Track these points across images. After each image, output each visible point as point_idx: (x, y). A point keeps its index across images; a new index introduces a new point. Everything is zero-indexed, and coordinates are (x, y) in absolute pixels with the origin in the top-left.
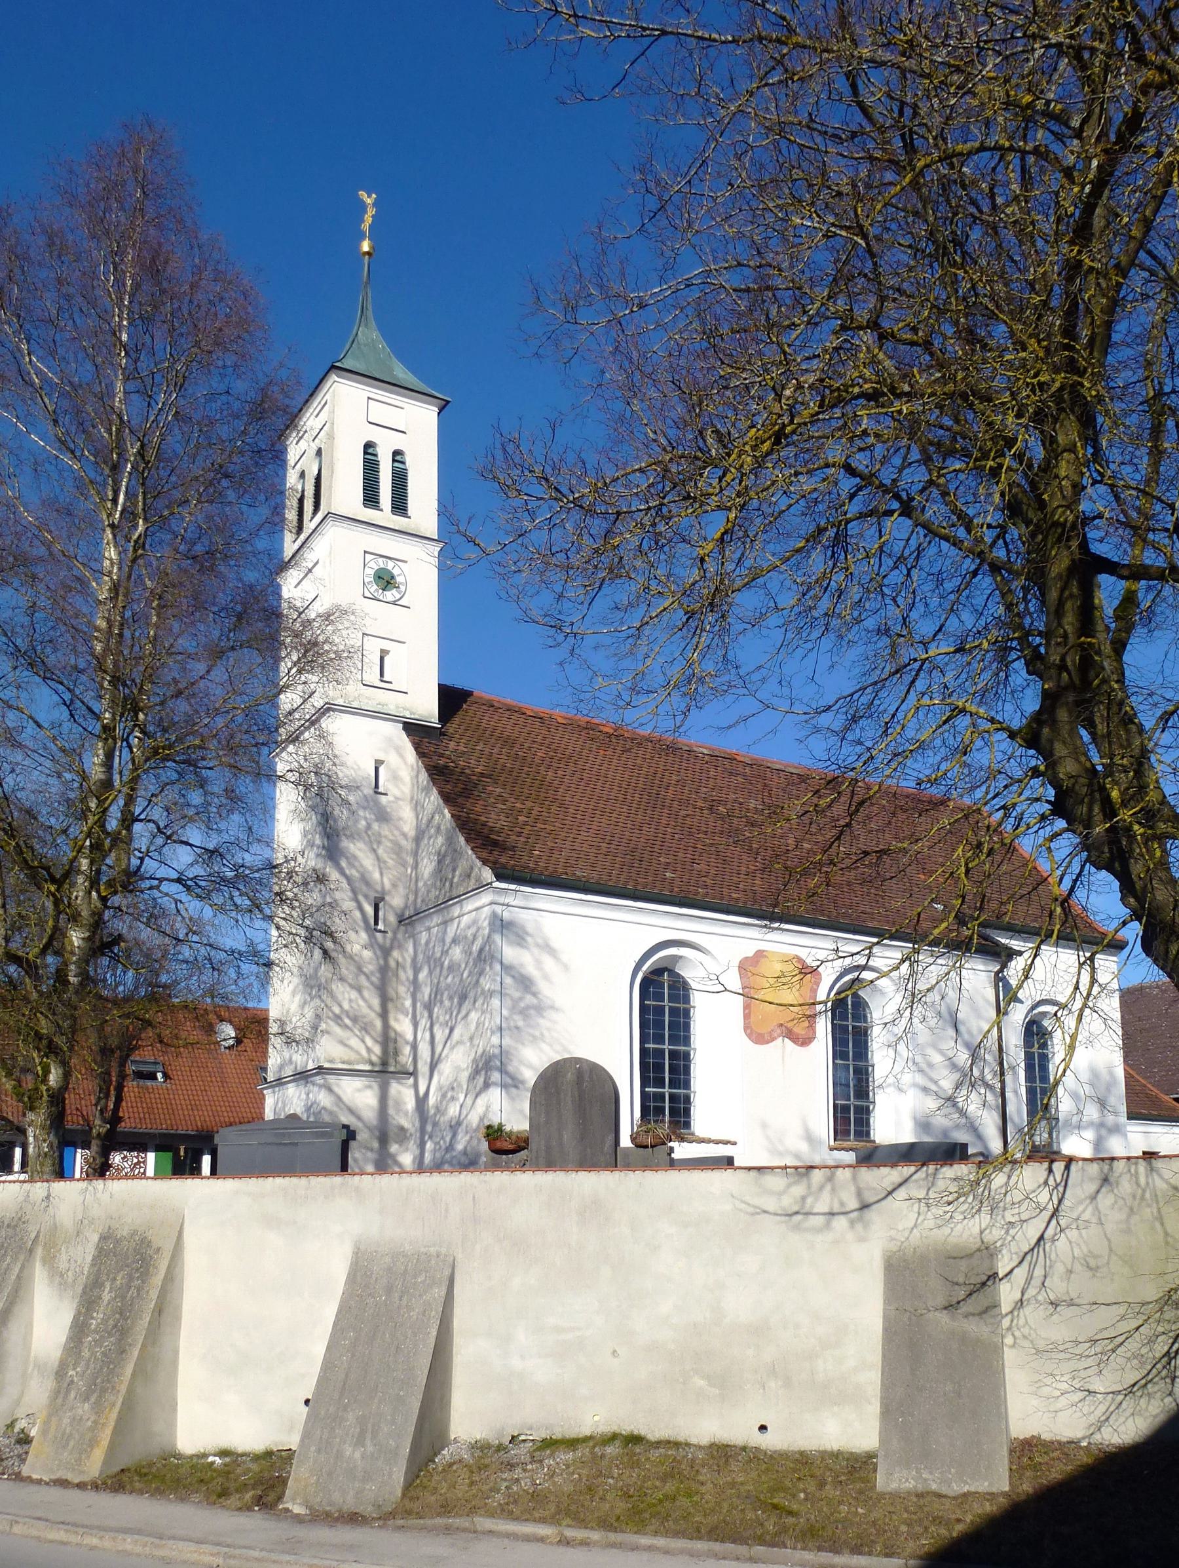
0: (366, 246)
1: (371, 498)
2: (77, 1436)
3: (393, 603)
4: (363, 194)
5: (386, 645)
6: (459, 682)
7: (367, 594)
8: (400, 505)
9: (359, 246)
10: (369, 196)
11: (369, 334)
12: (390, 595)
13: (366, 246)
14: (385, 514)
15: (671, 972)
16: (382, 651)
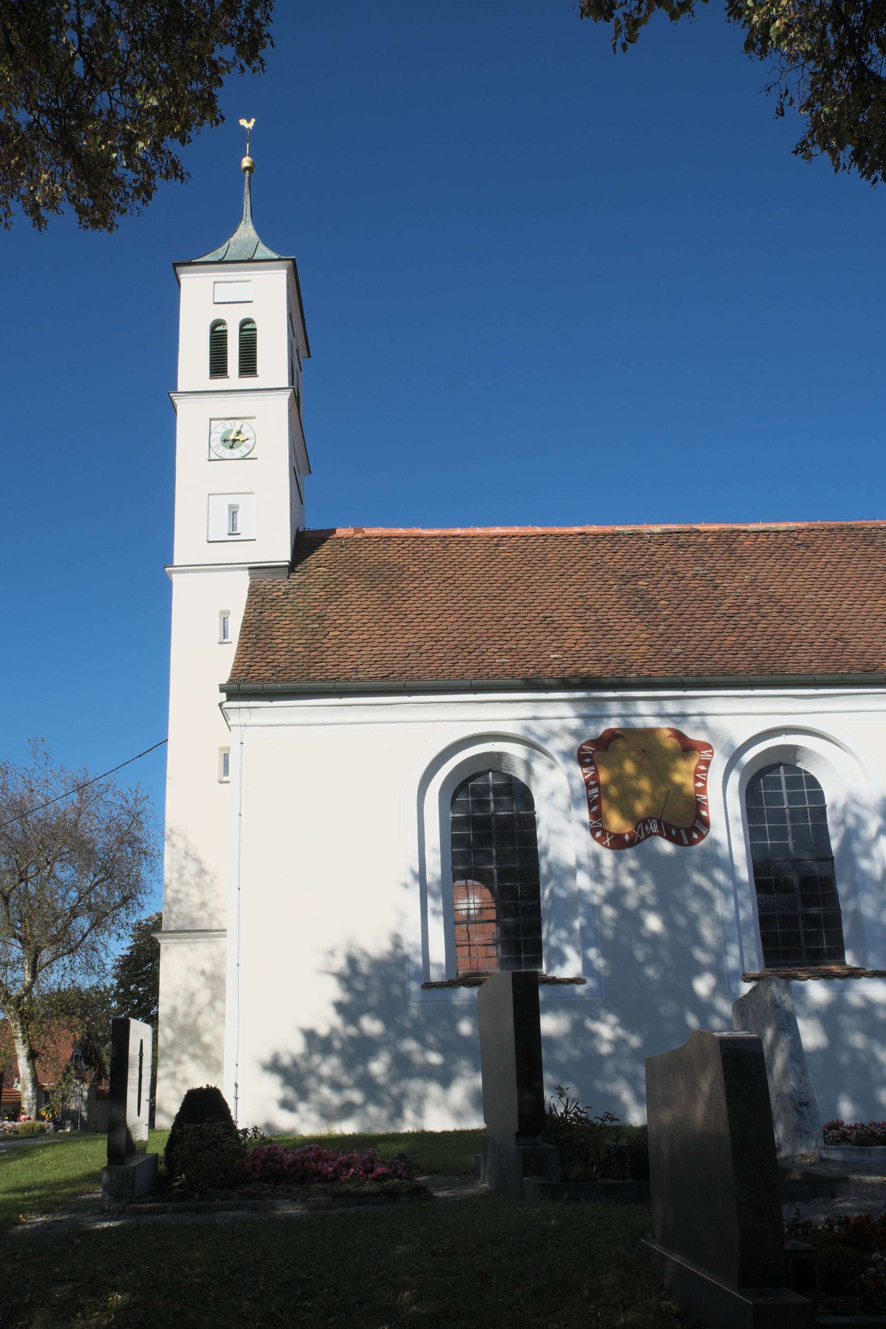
0: (246, 162)
1: (218, 368)
2: (700, 540)
3: (243, 458)
4: (243, 122)
5: (233, 499)
6: (312, 524)
7: (213, 457)
8: (248, 366)
9: (240, 163)
10: (249, 122)
11: (246, 233)
12: (237, 453)
13: (246, 162)
14: (233, 378)
15: (791, 767)
16: (231, 507)
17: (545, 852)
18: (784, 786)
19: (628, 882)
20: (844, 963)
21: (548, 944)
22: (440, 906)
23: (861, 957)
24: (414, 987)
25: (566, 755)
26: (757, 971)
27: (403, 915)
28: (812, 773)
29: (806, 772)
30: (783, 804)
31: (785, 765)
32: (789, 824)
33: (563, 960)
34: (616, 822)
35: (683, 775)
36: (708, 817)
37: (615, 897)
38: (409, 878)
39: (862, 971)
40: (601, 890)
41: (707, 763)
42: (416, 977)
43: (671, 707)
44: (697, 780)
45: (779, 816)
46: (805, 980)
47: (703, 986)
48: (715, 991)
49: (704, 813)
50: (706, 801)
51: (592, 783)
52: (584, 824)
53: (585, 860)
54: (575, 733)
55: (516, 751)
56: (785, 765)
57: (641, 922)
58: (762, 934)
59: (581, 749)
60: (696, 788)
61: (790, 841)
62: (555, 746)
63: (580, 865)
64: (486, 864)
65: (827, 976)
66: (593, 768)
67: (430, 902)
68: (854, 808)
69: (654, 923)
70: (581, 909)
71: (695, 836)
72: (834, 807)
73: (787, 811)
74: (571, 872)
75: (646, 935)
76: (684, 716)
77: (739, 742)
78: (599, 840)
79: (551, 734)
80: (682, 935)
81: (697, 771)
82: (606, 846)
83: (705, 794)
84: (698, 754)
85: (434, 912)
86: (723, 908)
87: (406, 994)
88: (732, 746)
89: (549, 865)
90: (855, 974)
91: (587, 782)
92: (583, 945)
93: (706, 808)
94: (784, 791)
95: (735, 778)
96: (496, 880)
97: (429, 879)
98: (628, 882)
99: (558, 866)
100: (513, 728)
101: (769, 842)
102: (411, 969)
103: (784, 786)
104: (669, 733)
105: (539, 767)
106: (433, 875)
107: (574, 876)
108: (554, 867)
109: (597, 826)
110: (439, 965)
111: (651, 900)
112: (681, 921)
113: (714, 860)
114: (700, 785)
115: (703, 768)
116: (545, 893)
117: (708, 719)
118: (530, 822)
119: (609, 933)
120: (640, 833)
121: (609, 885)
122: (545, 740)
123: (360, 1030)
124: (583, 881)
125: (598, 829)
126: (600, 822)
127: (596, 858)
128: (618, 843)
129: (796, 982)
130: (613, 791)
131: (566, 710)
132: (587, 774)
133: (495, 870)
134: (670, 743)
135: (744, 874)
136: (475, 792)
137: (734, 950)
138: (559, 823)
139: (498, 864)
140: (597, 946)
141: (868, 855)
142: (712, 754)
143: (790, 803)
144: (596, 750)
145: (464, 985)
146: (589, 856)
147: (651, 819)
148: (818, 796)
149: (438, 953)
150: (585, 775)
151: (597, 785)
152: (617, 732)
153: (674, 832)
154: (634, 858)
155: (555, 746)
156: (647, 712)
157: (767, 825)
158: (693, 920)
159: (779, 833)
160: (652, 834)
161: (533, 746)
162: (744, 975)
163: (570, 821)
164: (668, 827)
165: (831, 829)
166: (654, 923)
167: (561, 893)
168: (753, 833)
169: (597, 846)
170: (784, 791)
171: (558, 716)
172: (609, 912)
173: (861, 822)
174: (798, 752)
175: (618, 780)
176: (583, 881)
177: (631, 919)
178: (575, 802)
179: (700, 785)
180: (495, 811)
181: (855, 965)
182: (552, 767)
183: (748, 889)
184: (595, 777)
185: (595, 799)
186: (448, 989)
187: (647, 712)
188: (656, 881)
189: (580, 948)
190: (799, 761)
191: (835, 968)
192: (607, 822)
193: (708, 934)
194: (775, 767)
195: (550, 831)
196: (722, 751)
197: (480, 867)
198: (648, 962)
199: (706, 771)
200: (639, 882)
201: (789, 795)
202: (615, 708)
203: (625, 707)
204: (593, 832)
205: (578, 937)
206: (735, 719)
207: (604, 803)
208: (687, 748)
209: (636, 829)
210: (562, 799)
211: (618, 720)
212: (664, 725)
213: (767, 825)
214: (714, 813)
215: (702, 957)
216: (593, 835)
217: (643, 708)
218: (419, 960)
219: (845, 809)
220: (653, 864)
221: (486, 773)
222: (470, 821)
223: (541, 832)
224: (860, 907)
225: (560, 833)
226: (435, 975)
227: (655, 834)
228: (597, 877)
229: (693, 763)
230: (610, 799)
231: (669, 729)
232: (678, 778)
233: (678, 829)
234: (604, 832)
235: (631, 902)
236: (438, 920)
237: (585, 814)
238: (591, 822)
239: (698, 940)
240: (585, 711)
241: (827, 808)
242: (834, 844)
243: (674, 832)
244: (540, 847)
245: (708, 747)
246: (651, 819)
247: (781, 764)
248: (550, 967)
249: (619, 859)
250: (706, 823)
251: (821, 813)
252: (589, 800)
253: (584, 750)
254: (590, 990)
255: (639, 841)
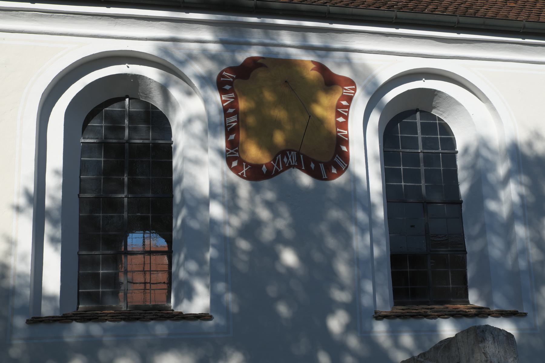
15: (427, 114)
17: (180, 180)
18: (419, 131)
19: (264, 214)
20: (468, 302)
21: (177, 276)
22: (58, 234)
23: (487, 296)
24: (20, 322)
25: (204, 80)
26: (388, 309)
27: (11, 243)
28: (446, 121)
29: (440, 119)
30: (418, 149)
31: (421, 112)
32: (422, 168)
33: (189, 293)
34: (254, 153)
35: (324, 108)
36: (348, 153)
37: (250, 230)
38: (22, 201)
39: (487, 311)
40: (235, 221)
41: (350, 99)
42: (22, 310)
43: (315, 40)
44: (339, 114)
45: (414, 159)
46: (435, 318)
47: (336, 323)
48: (348, 328)
49: (344, 148)
50: (347, 136)
51: (231, 111)
52: (220, 152)
53: (219, 190)
54: (213, 57)
55: (151, 73)
56: (421, 112)
57: (276, 257)
58: (393, 273)
59: (221, 75)
60: (338, 123)
61: (423, 184)
62: (193, 70)
63: (213, 196)
64: (116, 192)
65: (455, 315)
66: (232, 95)
67: (48, 229)
68: (485, 153)
69: (289, 257)
70: (213, 241)
71: (334, 171)
72: (466, 150)
73: (421, 155)
74: (205, 203)
75: (282, 270)
76: (328, 50)
77: (384, 77)
78: (235, 170)
79: (191, 57)
80: (319, 274)
81: (339, 106)
82: (242, 176)
83: (347, 130)
84: (340, 89)
85: (53, 240)
86: (360, 242)
87: (10, 330)
88: (375, 83)
89: (183, 193)
90: (482, 313)
91: (225, 109)
92: (213, 278)
93: (347, 146)
94: (420, 136)
95: (375, 118)
96: (126, 208)
97: (48, 203)
98: (264, 214)
99: (193, 197)
100: (146, 48)
101: (403, 184)
102: (17, 302)
103: (419, 131)
104: (312, 66)
105: (175, 94)
106: (53, 198)
107: (208, 205)
108: (188, 196)
109: (233, 156)
110: (51, 298)
111: (288, 234)
112: (317, 256)
113: (355, 196)
114: (341, 119)
115: (344, 103)
116: (178, 222)
117: (355, 56)
118: (167, 151)
119: (242, 267)
120: (278, 165)
121: (244, 216)
122: (183, 63)
123: (505, 182)
124: (216, 210)
125: (235, 159)
126: (237, 151)
127: (232, 189)
128: (255, 174)
129: (426, 320)
130: (251, 120)
131: (206, 34)
132: (226, 101)
133: (126, 200)
134: (312, 74)
135: (380, 213)
136: (109, 117)
137: (368, 287)
138: (195, 152)
139: (129, 192)
140: (226, 281)
141: (496, 197)
142: (355, 90)
143: (424, 147)
144: (237, 78)
145: (76, 320)
146: (224, 186)
147: (290, 151)
148: (450, 142)
149: (52, 282)
150: (223, 102)
151: (236, 113)
152: (259, 61)
153: (313, 166)
154: (271, 190)
155: (193, 70)
156: (290, 41)
157: (402, 167)
158: (330, 256)
159: (414, 176)
160: (290, 166)
161: (170, 68)
162: (376, 312)
163: (206, 150)
164: (308, 160)
165: (461, 174)
166: (289, 257)
167: (194, 224)
168: (388, 175)
169: (233, 176)
170: (420, 136)
171: (198, 36)
172: (244, 245)
173: (491, 166)
174: (436, 97)
175: (259, 107)
176: (216, 210)
177: (268, 253)
178: (211, 128)
179: (341, 119)
180: (130, 138)
181: (479, 305)
182: (189, 94)
183: (383, 227)
184: (234, 105)
185: (233, 127)
186: (57, 325)
187: (290, 41)
188: (293, 214)
189: (209, 281)
190: (434, 108)
191: (461, 307)
192: (244, 152)
193: (343, 269)
194: (412, 113)
195: (185, 158)
196: (365, 88)
197: (110, 195)
198: (280, 297)
199: (348, 107)
200: (276, 214)
201: (424, 140)
202: (257, 36)
203: (267, 35)
204: (229, 161)
205: (207, 268)
206: (381, 56)
207: (242, 136)
208: (330, 81)
209: (274, 160)
210: (198, 127)
211: (260, 48)
212: (306, 58)
213: (402, 167)
214: (355, 151)
215: (341, 296)
216: (229, 163)
217: (286, 38)
218: (28, 292)
219: (478, 155)
220: (291, 196)
221: (123, 99)
222: (104, 146)
223: (176, 161)
224: (486, 248)
225: (197, 162)
226: (47, 310)
227: (294, 167)
228: (232, 207)
229: (335, 98)
230: (248, 129)
231: (313, 62)
232: (319, 110)
233: (317, 163)
234: (241, 162)
235: (267, 234)
236: (56, 249)
237: (222, 143)
238: (227, 151)
239: (331, 276)
240: (225, 36)
241: (458, 155)
242: (463, 189)
243: (313, 166)
244: (175, 177)
245: (351, 82)
246: (290, 151)
247: (417, 110)
248: (178, 302)
249: (256, 190)
250: (345, 157)
251: (451, 157)
252: (226, 127)
253: (224, 77)
254: (217, 326)
255: (277, 173)
